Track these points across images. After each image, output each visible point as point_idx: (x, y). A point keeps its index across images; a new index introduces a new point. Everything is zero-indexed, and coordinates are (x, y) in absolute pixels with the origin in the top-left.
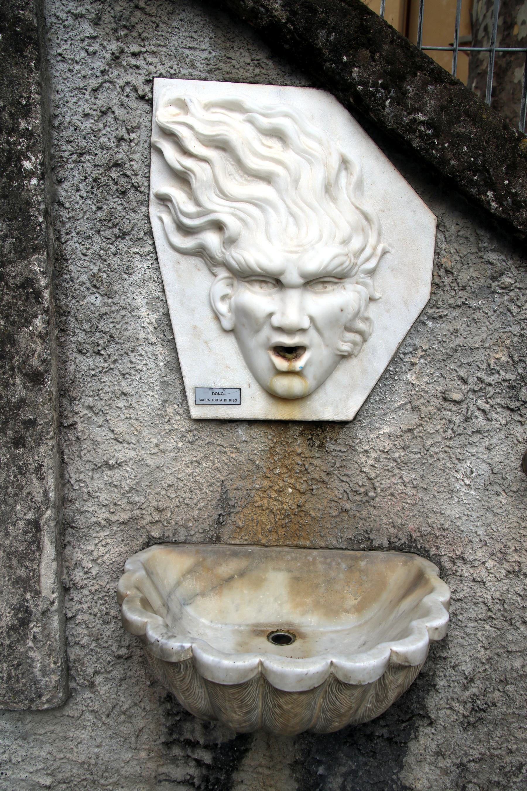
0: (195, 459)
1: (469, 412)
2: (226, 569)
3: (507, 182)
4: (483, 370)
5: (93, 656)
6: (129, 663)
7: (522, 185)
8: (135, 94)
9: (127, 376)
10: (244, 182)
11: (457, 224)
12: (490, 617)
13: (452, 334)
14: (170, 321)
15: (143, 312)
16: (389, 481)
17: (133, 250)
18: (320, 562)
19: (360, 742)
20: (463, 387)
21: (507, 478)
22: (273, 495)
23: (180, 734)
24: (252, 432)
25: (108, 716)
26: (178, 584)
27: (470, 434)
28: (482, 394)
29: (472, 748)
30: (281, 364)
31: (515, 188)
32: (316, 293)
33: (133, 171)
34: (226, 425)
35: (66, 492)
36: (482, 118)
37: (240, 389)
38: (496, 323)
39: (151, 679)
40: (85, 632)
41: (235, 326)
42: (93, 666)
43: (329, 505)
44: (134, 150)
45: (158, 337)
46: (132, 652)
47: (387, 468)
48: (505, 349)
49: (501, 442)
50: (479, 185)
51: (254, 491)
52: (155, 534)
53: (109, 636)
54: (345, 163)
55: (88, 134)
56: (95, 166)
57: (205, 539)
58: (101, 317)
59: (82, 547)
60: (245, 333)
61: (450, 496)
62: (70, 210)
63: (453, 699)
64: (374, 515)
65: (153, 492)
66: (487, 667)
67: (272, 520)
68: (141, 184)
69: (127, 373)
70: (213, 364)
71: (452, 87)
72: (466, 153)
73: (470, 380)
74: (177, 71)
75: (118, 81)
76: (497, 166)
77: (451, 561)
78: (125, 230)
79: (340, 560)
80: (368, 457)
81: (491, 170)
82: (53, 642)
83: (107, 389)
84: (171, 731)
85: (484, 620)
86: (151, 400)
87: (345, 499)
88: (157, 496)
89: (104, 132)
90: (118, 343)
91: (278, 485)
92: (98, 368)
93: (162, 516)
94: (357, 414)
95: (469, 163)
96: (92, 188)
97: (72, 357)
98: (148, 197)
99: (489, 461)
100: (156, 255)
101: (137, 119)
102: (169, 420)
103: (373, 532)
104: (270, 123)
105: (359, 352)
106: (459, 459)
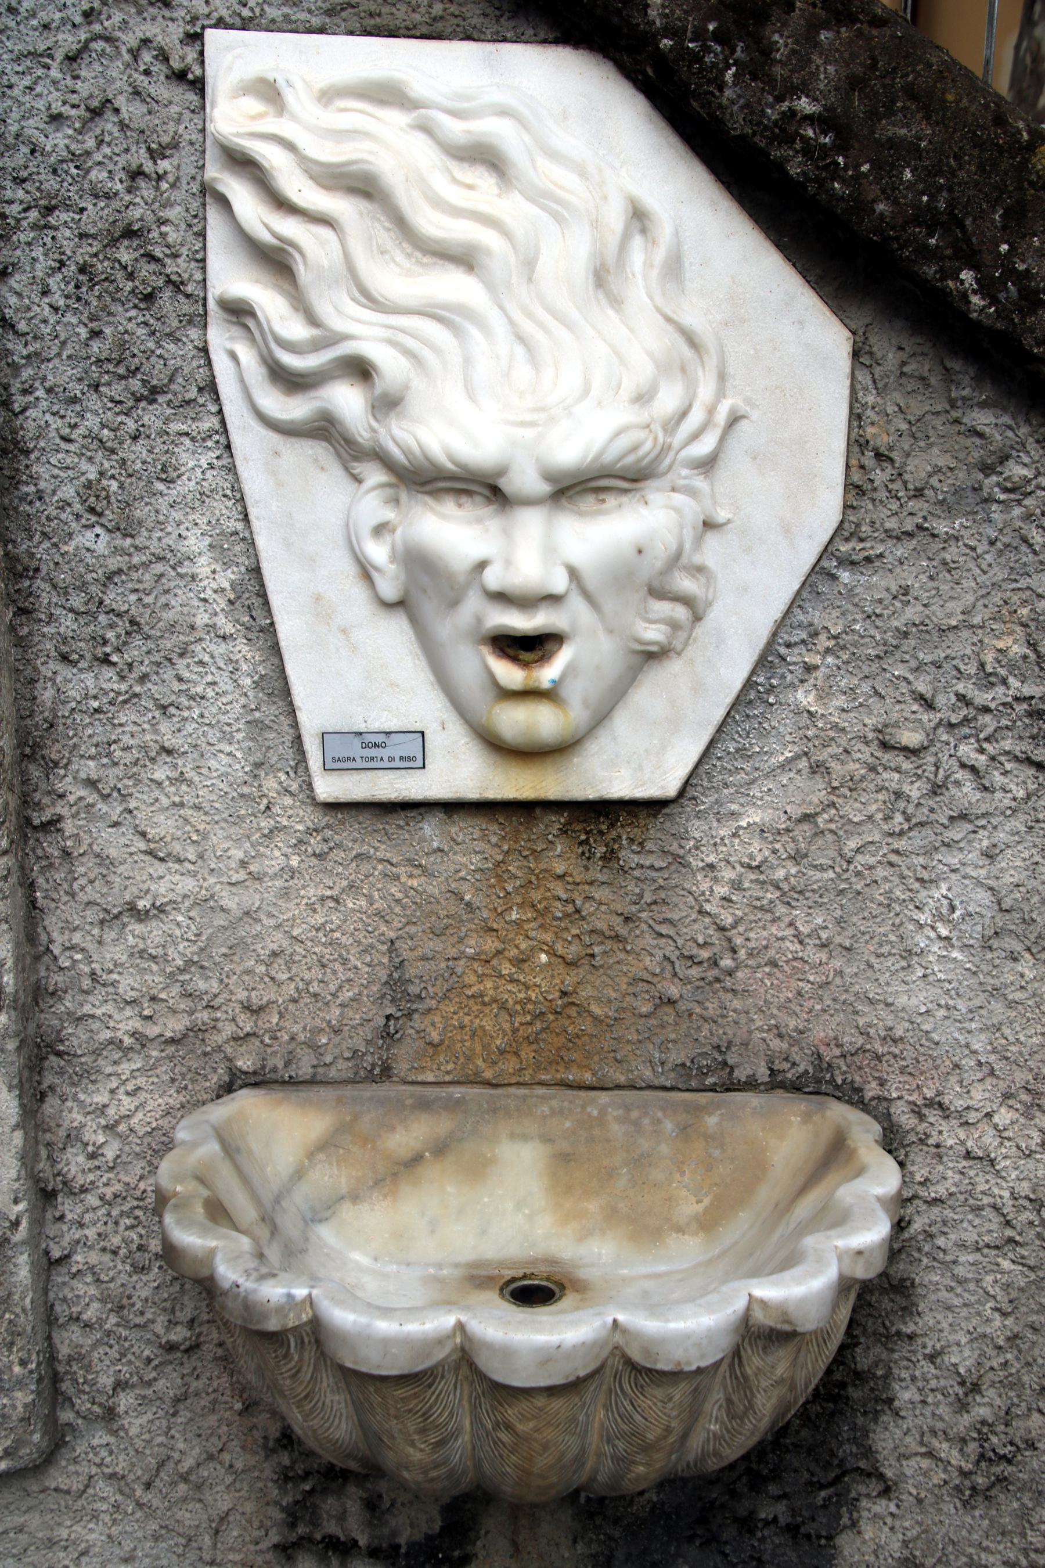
0: (329, 893)
1: (941, 772)
2: (409, 1136)
3: (1004, 247)
4: (969, 677)
5: (111, 1347)
6: (194, 1361)
7: (1042, 254)
8: (164, 68)
9: (172, 710)
10: (416, 269)
11: (900, 348)
12: (1011, 1240)
13: (895, 597)
14: (262, 585)
15: (203, 566)
16: (765, 933)
17: (176, 427)
18: (617, 1119)
19: (725, 1536)
20: (925, 717)
21: (1034, 921)
22: (507, 969)
23: (313, 1524)
24: (453, 830)
25: (148, 1486)
26: (299, 1174)
27: (945, 821)
28: (968, 731)
29: (986, 1549)
30: (510, 674)
31: (1023, 261)
32: (581, 514)
33: (168, 247)
34: (395, 816)
35: (43, 974)
36: (945, 101)
37: (423, 733)
38: (996, 569)
39: (245, 1396)
40: (92, 1291)
41: (407, 592)
42: (112, 1369)
43: (631, 990)
44: (168, 199)
45: (237, 621)
46: (199, 1334)
47: (758, 904)
48: (1018, 629)
49: (1016, 838)
50: (943, 258)
51: (462, 962)
52: (245, 1063)
53: (147, 1300)
54: (639, 217)
55: (62, 161)
56: (82, 236)
57: (356, 1074)
58: (109, 578)
59: (82, 1096)
60: (428, 607)
61: (904, 964)
62: (29, 338)
63: (934, 1432)
64: (735, 1011)
65: (239, 970)
66: (1009, 1356)
67: (507, 1026)
68: (186, 276)
69: (171, 704)
70: (362, 680)
71: (875, 32)
72: (910, 186)
73: (941, 700)
74: (257, 11)
75: (123, 37)
76: (983, 211)
77: (913, 1111)
78: (155, 382)
79: (660, 1114)
80: (716, 880)
81: (968, 222)
82: (17, 1315)
83: (127, 740)
84: (293, 1516)
85: (997, 1247)
86: (226, 762)
87: (668, 974)
88: (246, 978)
89: (98, 157)
90: (148, 637)
91: (517, 947)
92: (106, 694)
93: (260, 1023)
94: (687, 783)
95: (917, 206)
96: (77, 287)
97: (46, 672)
98: (205, 305)
99: (992, 883)
100: (227, 437)
101: (171, 127)
102: (268, 808)
103: (733, 1049)
104: (469, 132)
105: (686, 644)
106: (921, 880)
